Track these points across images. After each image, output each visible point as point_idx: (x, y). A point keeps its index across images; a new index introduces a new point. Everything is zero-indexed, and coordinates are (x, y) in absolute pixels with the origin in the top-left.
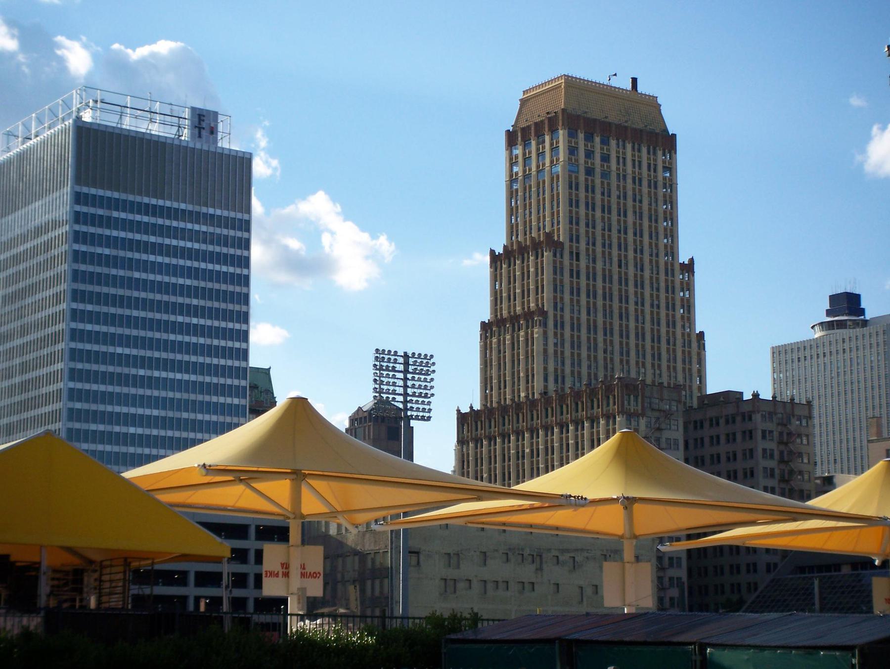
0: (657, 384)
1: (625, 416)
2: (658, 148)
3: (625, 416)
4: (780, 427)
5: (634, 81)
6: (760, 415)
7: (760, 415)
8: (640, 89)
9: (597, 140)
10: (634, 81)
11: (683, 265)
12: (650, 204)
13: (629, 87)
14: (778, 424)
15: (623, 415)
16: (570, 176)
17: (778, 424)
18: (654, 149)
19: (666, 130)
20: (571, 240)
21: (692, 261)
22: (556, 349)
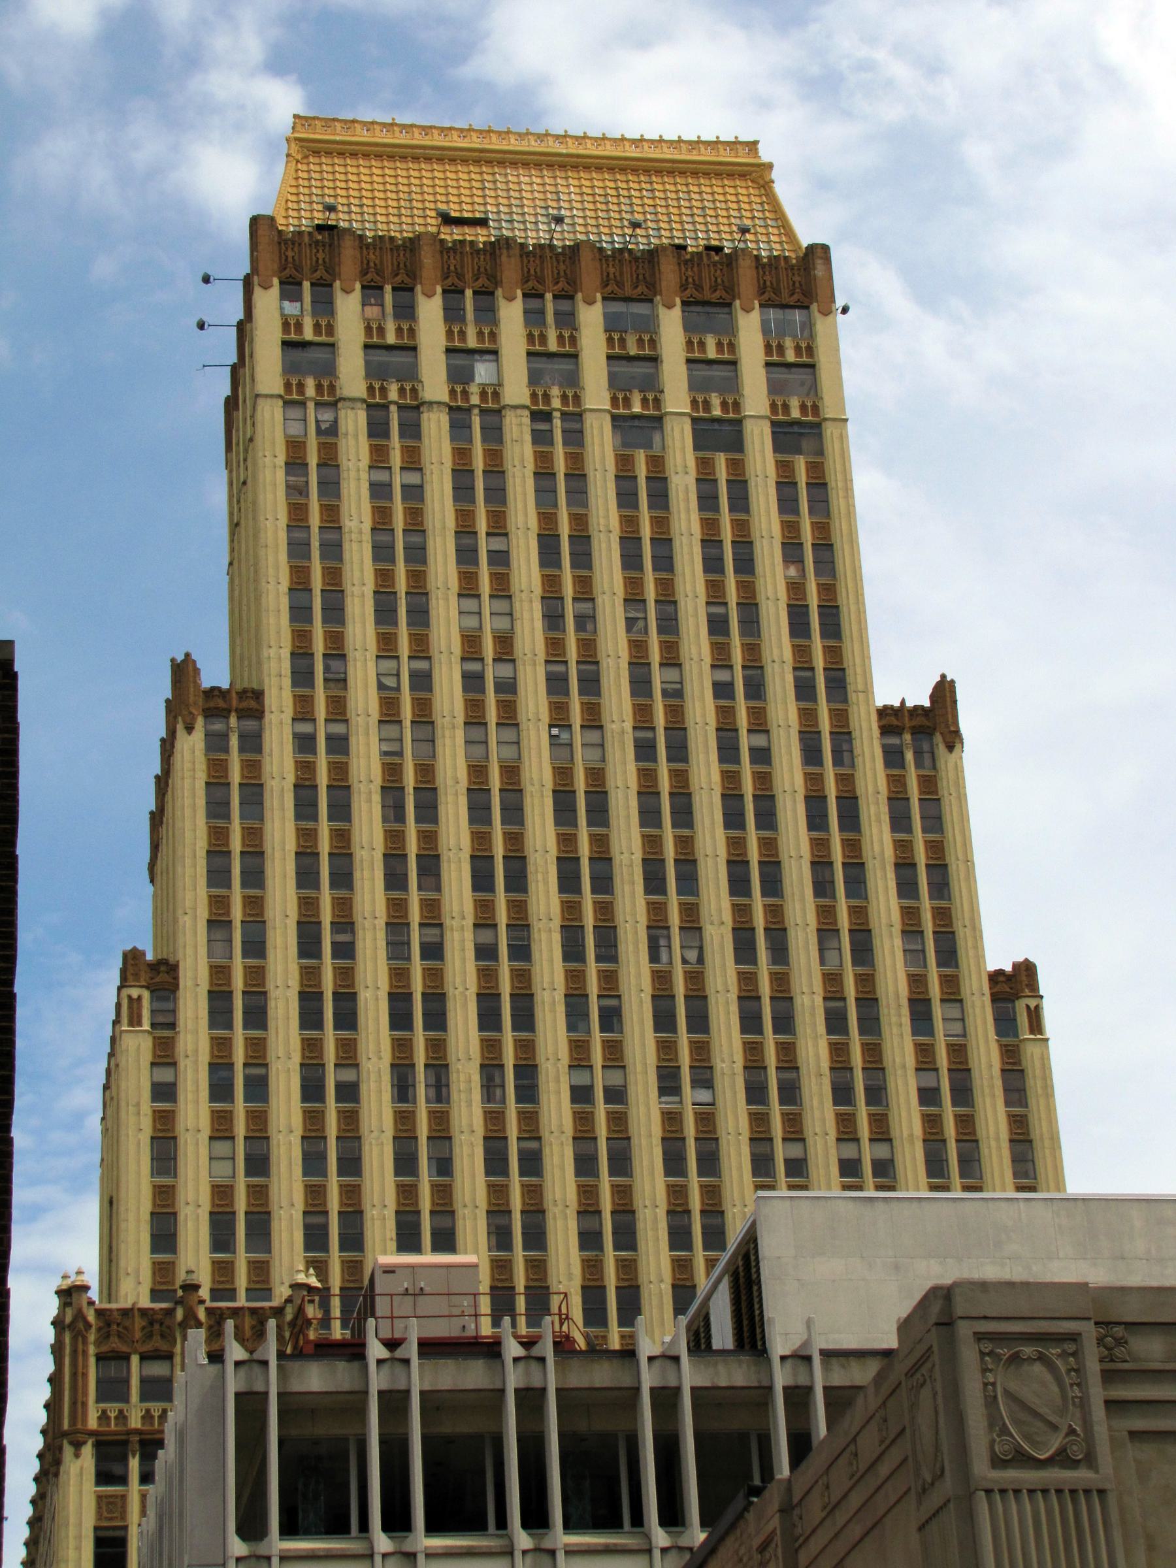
2: (658, 298)
21: (944, 691)
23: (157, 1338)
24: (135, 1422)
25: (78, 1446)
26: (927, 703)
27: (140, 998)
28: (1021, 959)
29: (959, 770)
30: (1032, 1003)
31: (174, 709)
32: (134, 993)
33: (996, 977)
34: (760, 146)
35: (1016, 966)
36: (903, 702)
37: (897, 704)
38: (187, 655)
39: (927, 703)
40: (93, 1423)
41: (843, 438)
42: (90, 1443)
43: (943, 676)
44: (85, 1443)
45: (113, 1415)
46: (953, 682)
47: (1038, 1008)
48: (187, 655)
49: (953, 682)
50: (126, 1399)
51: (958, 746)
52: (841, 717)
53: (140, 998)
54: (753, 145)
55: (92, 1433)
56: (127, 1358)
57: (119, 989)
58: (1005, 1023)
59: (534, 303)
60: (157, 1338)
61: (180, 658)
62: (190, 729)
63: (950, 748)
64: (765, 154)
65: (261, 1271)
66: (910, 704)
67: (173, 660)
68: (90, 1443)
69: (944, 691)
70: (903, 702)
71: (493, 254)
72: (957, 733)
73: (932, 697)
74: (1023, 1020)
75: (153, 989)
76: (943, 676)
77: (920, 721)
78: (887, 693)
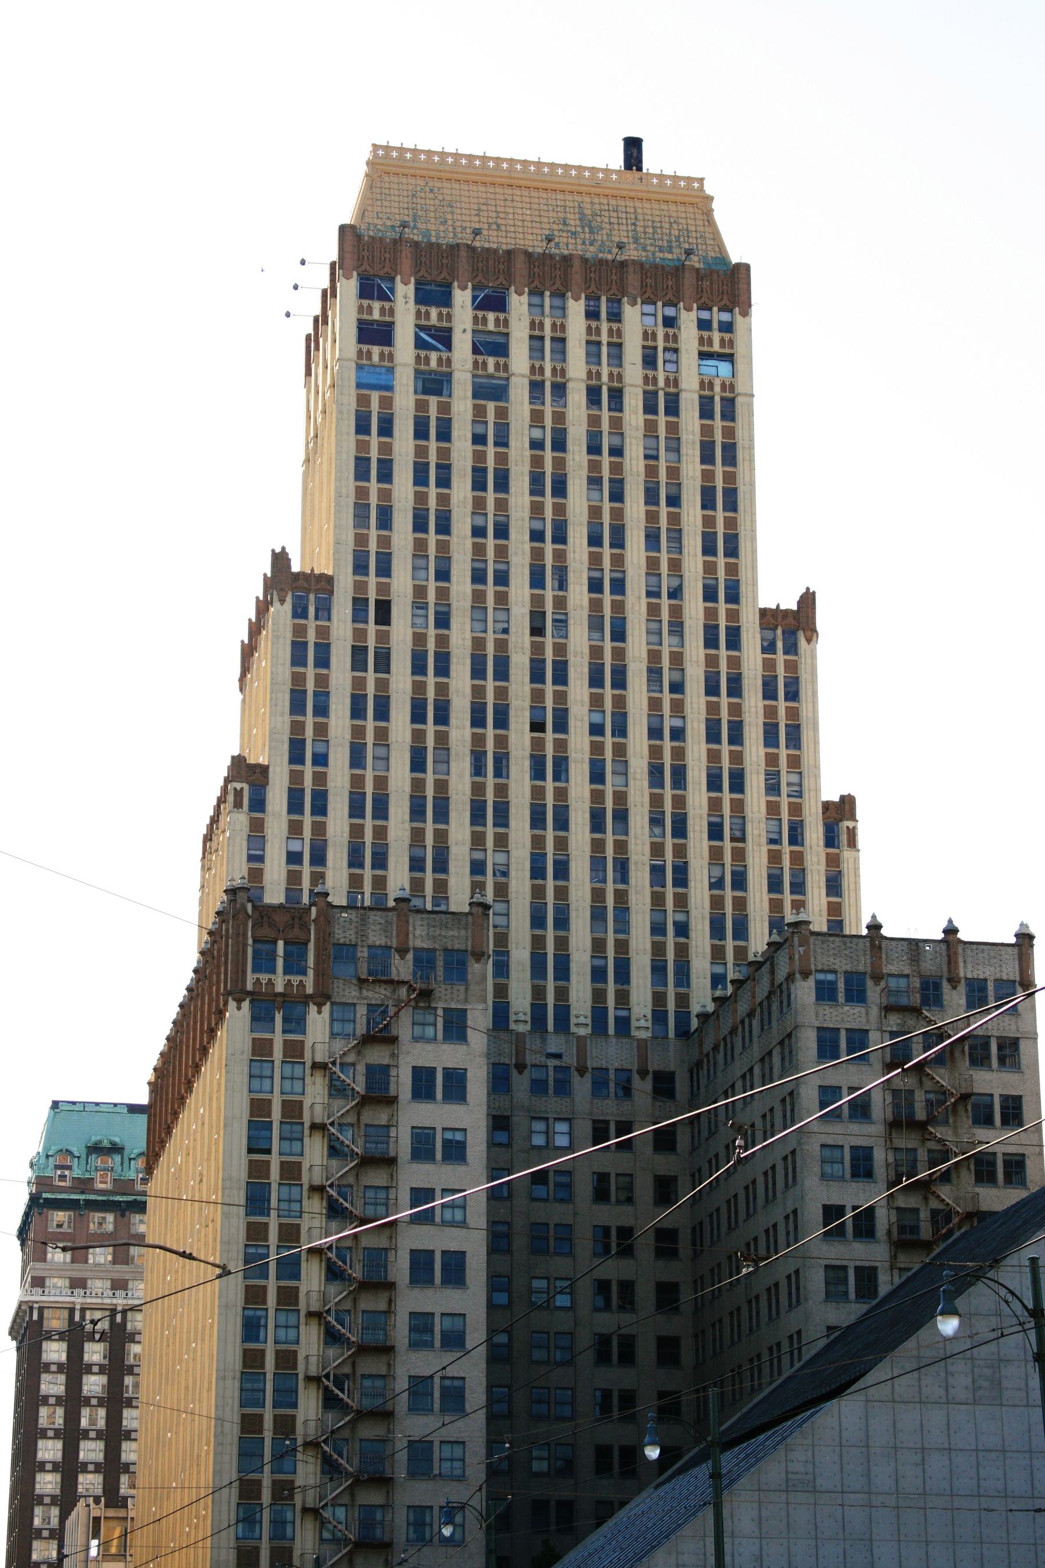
0: (391, 904)
1: (246, 1005)
2: (626, 299)
3: (246, 1005)
4: (894, 1021)
5: (633, 147)
6: (811, 982)
7: (811, 982)
8: (651, 162)
9: (462, 298)
10: (633, 147)
11: (770, 618)
12: (651, 457)
13: (616, 160)
14: (888, 1009)
15: (239, 1001)
16: (363, 401)
17: (888, 1009)
18: (615, 303)
19: (723, 258)
20: (360, 567)
21: (808, 600)
22: (660, 989)
23: (296, 929)
24: (279, 988)
25: (239, 1001)
26: (795, 608)
27: (242, 789)
28: (846, 794)
29: (814, 656)
30: (850, 824)
31: (270, 584)
32: (238, 786)
33: (827, 806)
34: (705, 182)
35: (842, 797)
36: (778, 606)
37: (774, 607)
38: (283, 548)
39: (795, 608)
40: (249, 987)
41: (750, 406)
42: (248, 1000)
43: (808, 589)
44: (244, 1000)
45: (264, 982)
46: (814, 593)
47: (854, 828)
48: (283, 548)
49: (814, 593)
50: (273, 971)
51: (814, 638)
52: (733, 616)
53: (242, 789)
54: (701, 180)
55: (249, 993)
56: (274, 942)
57: (227, 781)
58: (831, 840)
59: (536, 300)
60: (296, 929)
61: (278, 550)
62: (282, 601)
63: (809, 641)
64: (709, 189)
65: (380, 883)
66: (782, 607)
67: (273, 551)
68: (248, 1000)
69: (808, 600)
70: (778, 606)
71: (509, 260)
72: (814, 630)
73: (799, 603)
74: (844, 838)
75: (251, 784)
76: (808, 589)
77: (790, 620)
78: (767, 599)
